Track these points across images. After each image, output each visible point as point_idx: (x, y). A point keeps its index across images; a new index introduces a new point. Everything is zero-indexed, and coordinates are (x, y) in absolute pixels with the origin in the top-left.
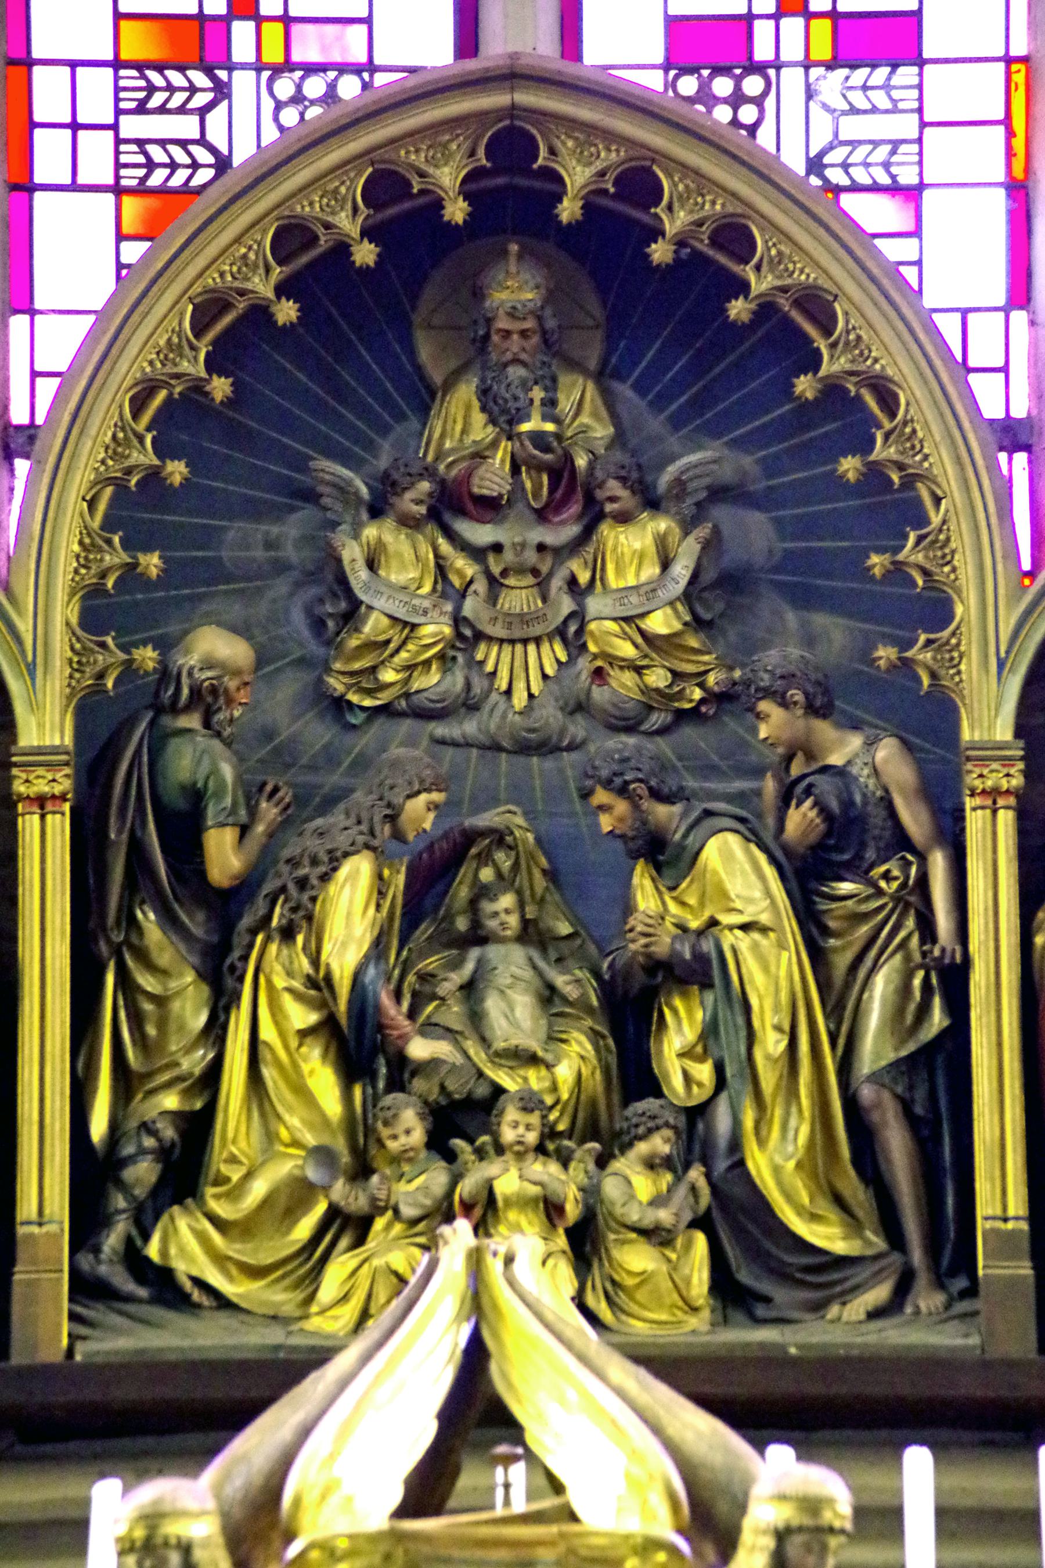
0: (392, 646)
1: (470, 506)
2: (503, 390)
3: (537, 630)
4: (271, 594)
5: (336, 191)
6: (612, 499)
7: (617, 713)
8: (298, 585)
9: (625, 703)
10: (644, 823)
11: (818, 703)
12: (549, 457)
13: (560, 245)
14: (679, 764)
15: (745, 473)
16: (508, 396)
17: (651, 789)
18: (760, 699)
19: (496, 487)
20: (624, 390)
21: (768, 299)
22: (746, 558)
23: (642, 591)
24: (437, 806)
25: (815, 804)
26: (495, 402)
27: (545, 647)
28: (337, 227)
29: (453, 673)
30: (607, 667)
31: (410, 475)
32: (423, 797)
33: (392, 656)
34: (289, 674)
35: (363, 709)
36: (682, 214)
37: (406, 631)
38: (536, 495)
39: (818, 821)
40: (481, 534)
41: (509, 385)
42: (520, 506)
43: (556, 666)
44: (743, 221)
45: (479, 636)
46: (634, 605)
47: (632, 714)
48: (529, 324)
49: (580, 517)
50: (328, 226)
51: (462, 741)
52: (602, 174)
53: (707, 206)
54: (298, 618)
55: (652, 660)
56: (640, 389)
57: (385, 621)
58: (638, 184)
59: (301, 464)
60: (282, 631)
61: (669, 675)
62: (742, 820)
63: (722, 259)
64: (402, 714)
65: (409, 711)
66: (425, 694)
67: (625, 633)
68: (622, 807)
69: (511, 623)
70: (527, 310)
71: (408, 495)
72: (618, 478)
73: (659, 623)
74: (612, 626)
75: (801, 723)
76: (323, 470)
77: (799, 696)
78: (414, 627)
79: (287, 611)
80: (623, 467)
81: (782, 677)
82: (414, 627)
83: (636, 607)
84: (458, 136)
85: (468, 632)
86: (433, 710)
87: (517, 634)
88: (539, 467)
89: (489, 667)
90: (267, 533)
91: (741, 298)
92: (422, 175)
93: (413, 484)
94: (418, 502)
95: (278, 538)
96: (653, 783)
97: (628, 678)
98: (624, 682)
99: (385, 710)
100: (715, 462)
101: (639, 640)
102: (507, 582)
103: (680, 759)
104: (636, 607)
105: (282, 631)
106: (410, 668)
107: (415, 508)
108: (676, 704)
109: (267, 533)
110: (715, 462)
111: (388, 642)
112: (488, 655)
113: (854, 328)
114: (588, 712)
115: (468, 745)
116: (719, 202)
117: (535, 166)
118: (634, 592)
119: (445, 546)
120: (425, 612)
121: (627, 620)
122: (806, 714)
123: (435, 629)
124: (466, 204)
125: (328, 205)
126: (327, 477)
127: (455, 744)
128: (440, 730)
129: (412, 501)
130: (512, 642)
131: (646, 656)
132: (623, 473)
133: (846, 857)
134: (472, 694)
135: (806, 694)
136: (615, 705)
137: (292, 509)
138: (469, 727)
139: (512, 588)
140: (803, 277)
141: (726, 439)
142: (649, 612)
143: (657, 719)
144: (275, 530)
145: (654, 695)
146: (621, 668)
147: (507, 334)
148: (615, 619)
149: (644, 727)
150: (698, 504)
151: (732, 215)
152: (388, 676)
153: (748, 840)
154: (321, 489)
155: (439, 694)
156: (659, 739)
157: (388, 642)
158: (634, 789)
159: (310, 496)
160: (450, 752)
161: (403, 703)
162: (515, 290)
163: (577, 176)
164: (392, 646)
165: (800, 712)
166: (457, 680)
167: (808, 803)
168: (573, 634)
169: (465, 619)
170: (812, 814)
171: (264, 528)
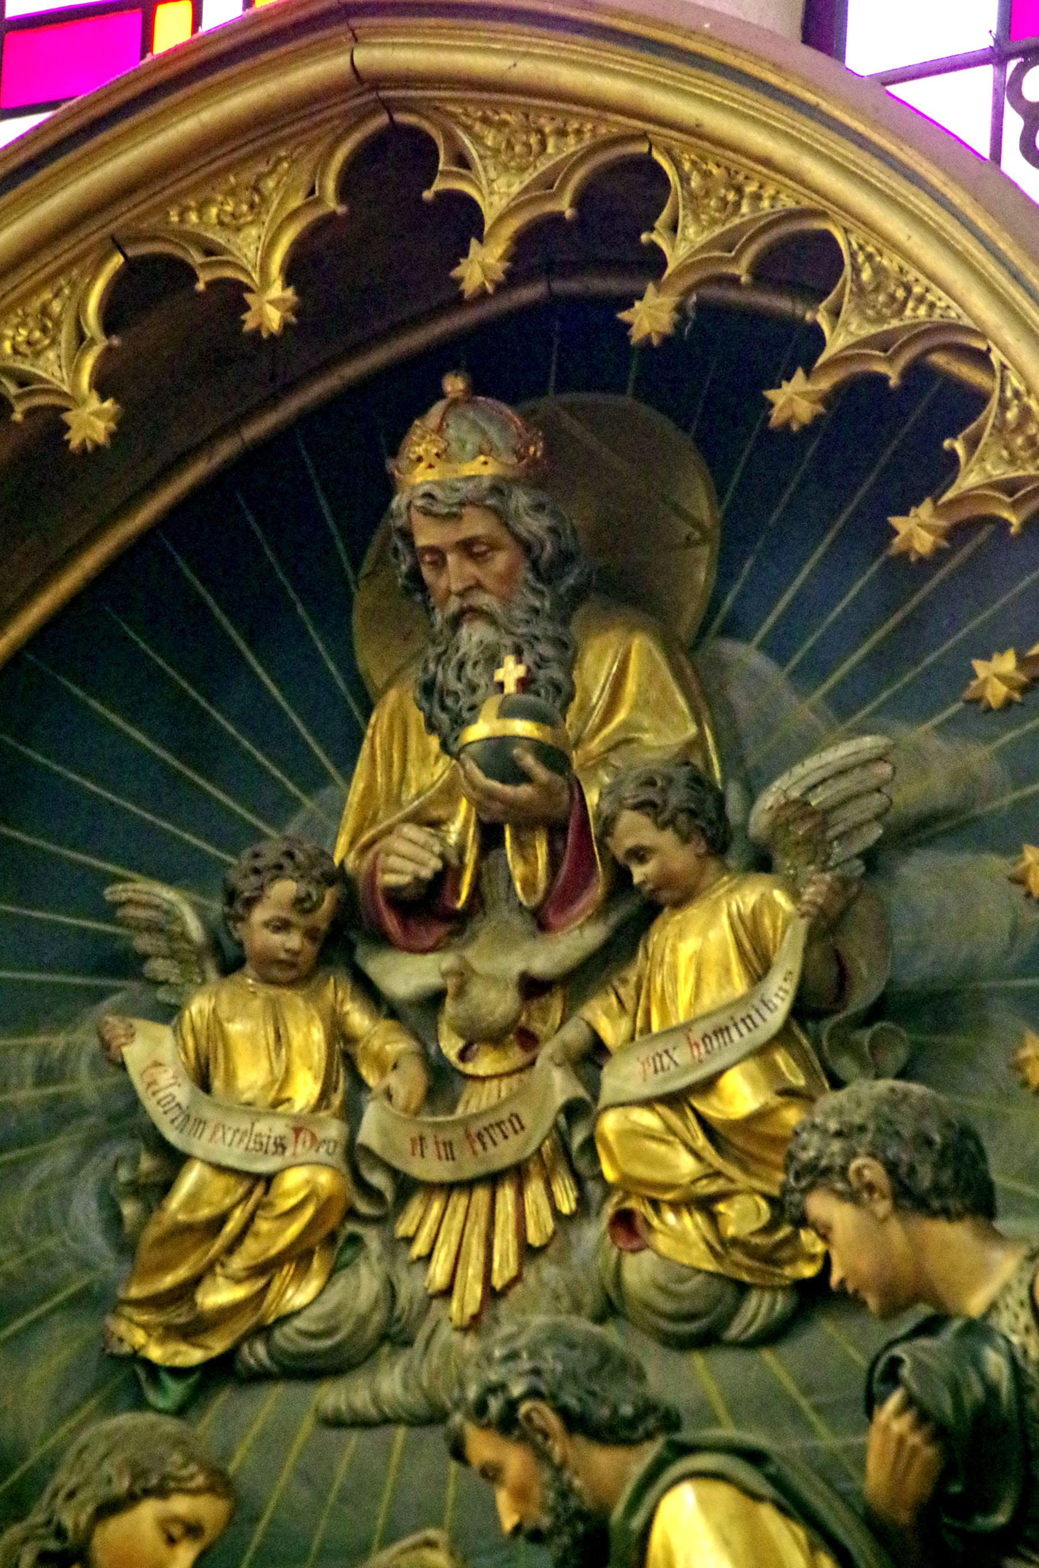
0: (231, 1227)
1: (391, 922)
2: (451, 674)
3: (504, 1153)
4: (42, 1170)
5: (45, 311)
6: (640, 854)
7: (668, 1306)
8: (92, 1145)
9: (682, 1280)
10: (565, 1493)
11: (925, 1177)
12: (524, 791)
13: (647, 393)
14: (804, 1403)
15: (975, 779)
16: (459, 687)
17: (563, 1412)
18: (806, 1191)
19: (410, 867)
20: (746, 655)
21: (856, 368)
22: (964, 952)
23: (696, 1035)
24: (193, 1530)
25: (909, 1402)
26: (444, 708)
27: (535, 1190)
28: (41, 380)
29: (356, 1273)
30: (644, 1210)
31: (256, 871)
32: (148, 1511)
33: (231, 1249)
34: (59, 1328)
35: (178, 1373)
36: (691, 231)
37: (259, 1191)
38: (529, 885)
39: (915, 1439)
40: (405, 975)
41: (461, 665)
42: (504, 912)
43: (550, 1225)
44: (818, 225)
45: (407, 1187)
46: (684, 1066)
47: (700, 1304)
48: (477, 525)
49: (602, 911)
50: (23, 380)
51: (373, 1412)
52: (547, 184)
53: (745, 209)
54: (85, 1211)
55: (732, 1180)
56: (777, 649)
57: (208, 1173)
58: (623, 196)
59: (88, 892)
60: (50, 1243)
61: (763, 1205)
62: (755, 1457)
63: (783, 304)
64: (260, 1377)
65: (275, 1369)
66: (299, 1323)
67: (670, 1129)
68: (514, 1460)
69: (449, 1145)
70: (456, 497)
71: (260, 915)
72: (639, 807)
73: (740, 1096)
74: (647, 1119)
75: (895, 1231)
76: (129, 901)
77: (874, 1172)
78: (269, 1180)
79: (65, 1198)
80: (651, 783)
81: (839, 1134)
82: (269, 1180)
83: (687, 1070)
84: (280, 160)
85: (378, 1179)
86: (311, 1355)
87: (470, 1169)
88: (527, 822)
89: (419, 1248)
90: (45, 1050)
91: (800, 373)
92: (210, 250)
93: (261, 888)
94: (282, 926)
95: (64, 1058)
96: (571, 1401)
97: (692, 1224)
98: (679, 1239)
99: (220, 1371)
100: (880, 759)
101: (701, 1141)
102: (469, 1068)
103: (808, 1390)
104: (687, 1070)
105: (50, 1243)
106: (265, 1269)
107: (277, 939)
108: (788, 1271)
109: (45, 1050)
110: (880, 759)
111: (220, 1221)
112: (419, 1219)
113: (1017, 394)
114: (625, 1317)
115: (386, 1421)
116: (769, 191)
117: (428, 195)
118: (680, 1036)
119: (358, 1019)
120: (281, 1146)
121: (675, 1100)
122: (897, 1207)
123: (305, 1179)
124: (290, 293)
125: (29, 343)
126: (141, 913)
127: (361, 1423)
128: (331, 1396)
129: (266, 924)
130: (467, 1186)
131: (718, 1174)
132: (650, 794)
133: (1000, 1518)
134: (397, 1313)
135: (891, 1168)
136: (662, 1289)
137: (99, 995)
138: (390, 1383)
139: (484, 1079)
140: (922, 311)
141: (936, 720)
142: (720, 1073)
143: (759, 1309)
144: (59, 1042)
145: (738, 1256)
146: (675, 1207)
147: (438, 555)
148: (647, 1103)
149: (733, 1332)
150: (870, 857)
151: (790, 215)
152: (219, 1295)
153: (756, 1497)
154: (143, 943)
155: (319, 1318)
156: (767, 1356)
157: (220, 1221)
158: (528, 1417)
159: (125, 964)
160: (354, 1439)
161: (260, 1349)
162: (450, 461)
163: (498, 192)
164: (231, 1227)
165: (883, 1207)
166: (364, 1284)
167: (895, 1400)
168: (570, 1147)
169: (367, 1151)
170: (901, 1425)
171: (37, 1041)
